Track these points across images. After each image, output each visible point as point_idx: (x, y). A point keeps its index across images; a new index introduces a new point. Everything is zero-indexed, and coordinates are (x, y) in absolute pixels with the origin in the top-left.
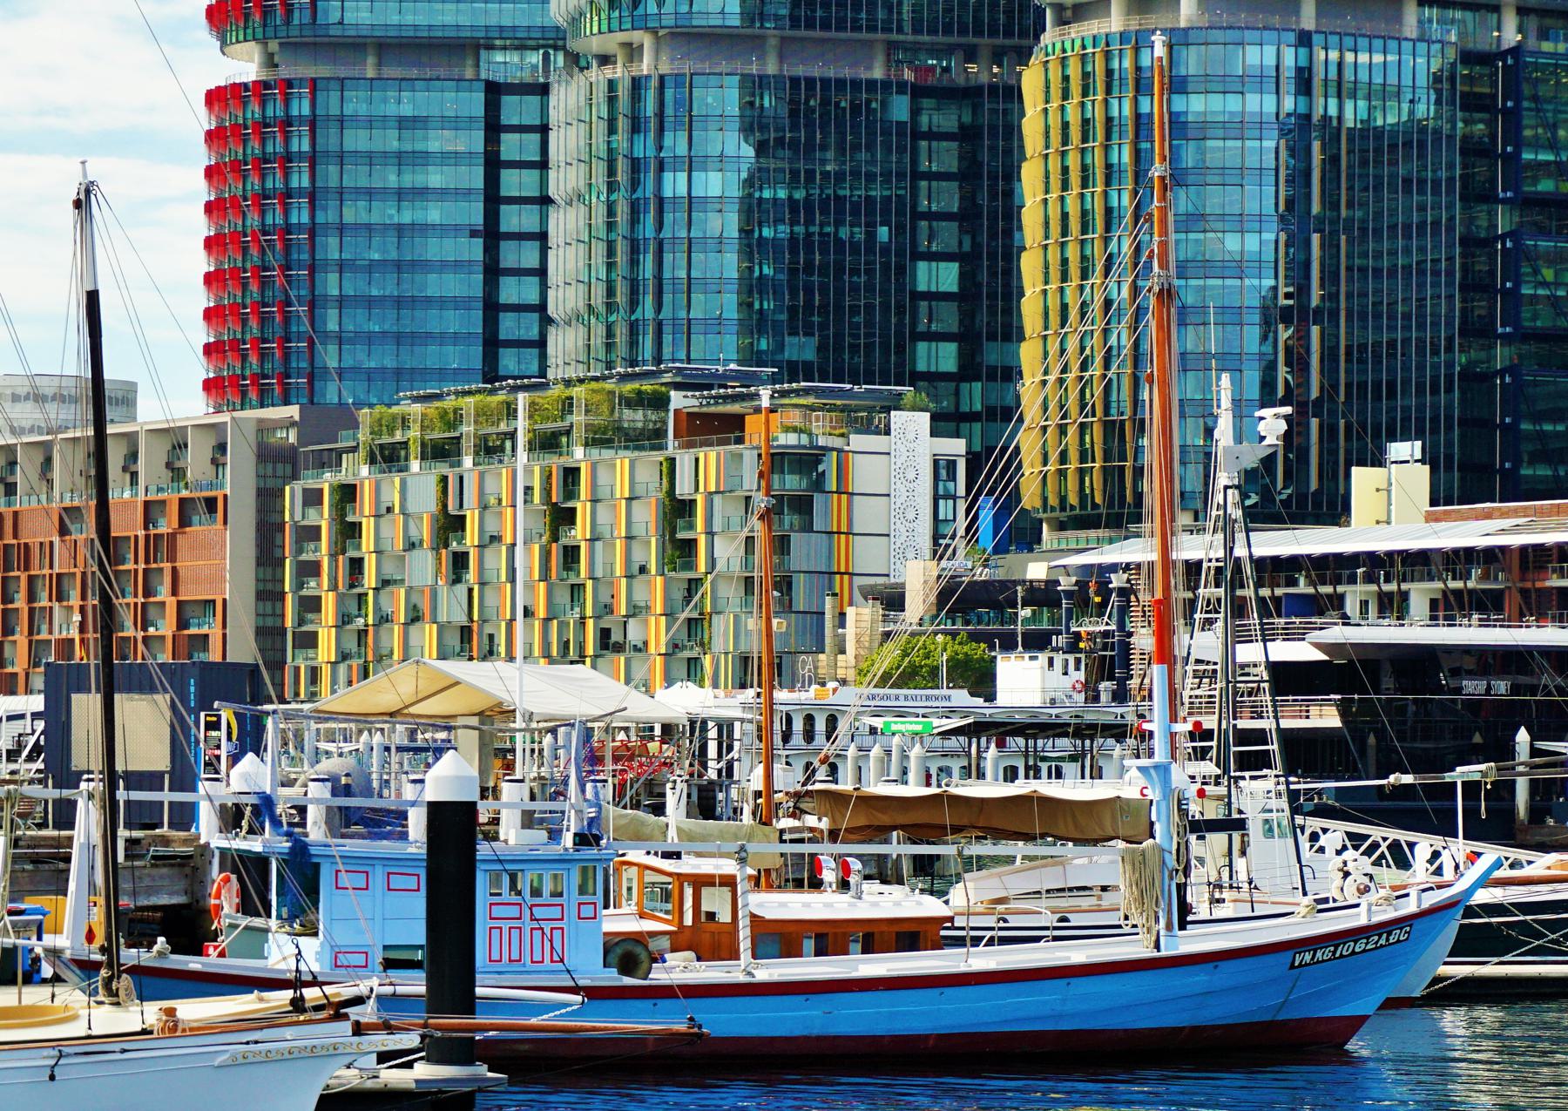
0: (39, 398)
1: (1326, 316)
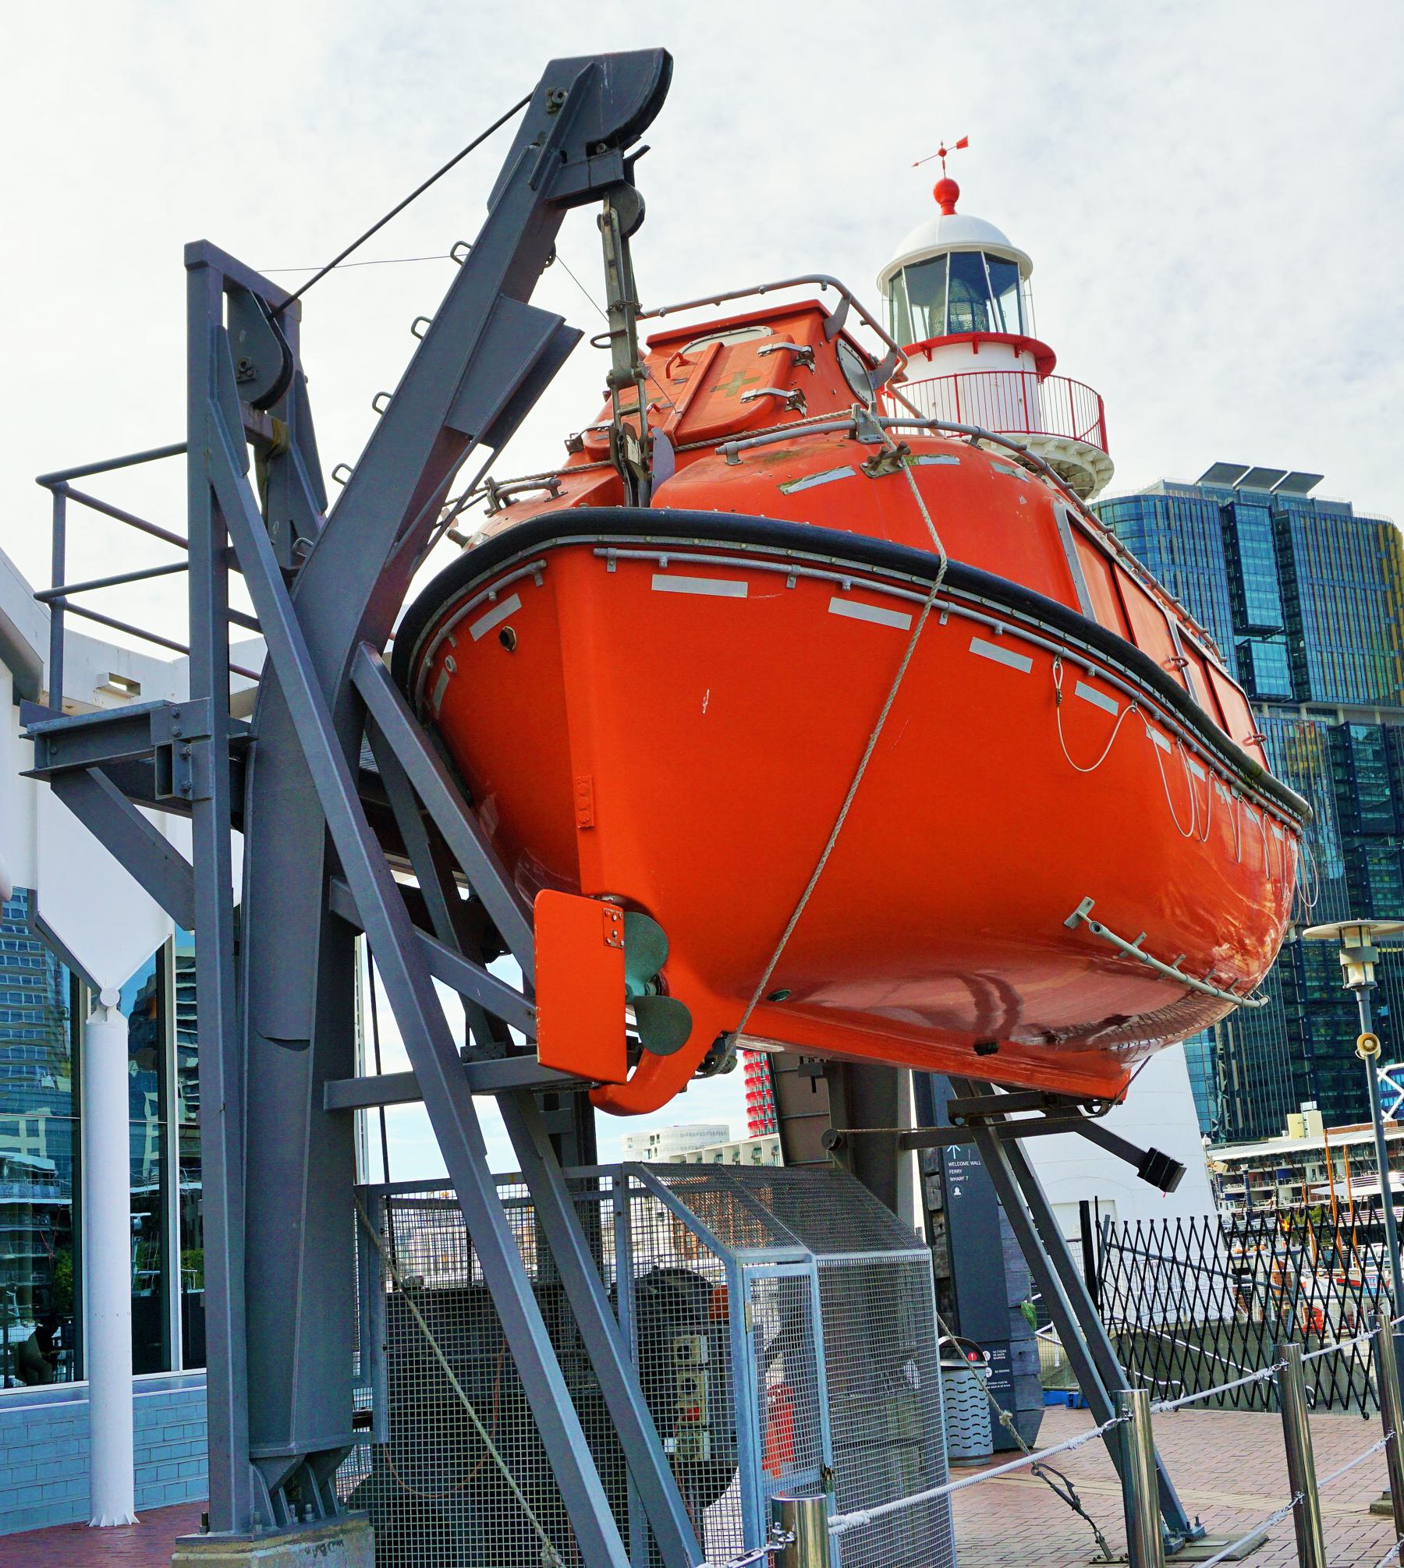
0: (702, 1134)
1: (1237, 1054)
